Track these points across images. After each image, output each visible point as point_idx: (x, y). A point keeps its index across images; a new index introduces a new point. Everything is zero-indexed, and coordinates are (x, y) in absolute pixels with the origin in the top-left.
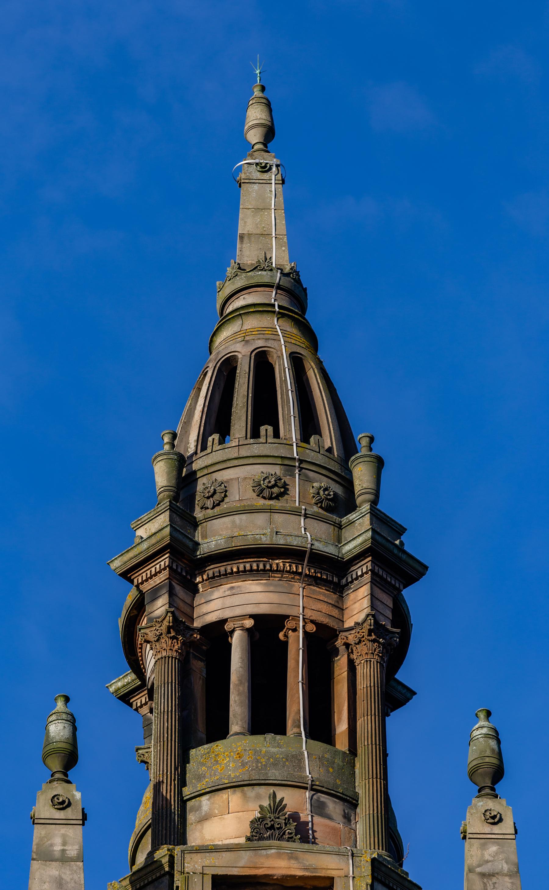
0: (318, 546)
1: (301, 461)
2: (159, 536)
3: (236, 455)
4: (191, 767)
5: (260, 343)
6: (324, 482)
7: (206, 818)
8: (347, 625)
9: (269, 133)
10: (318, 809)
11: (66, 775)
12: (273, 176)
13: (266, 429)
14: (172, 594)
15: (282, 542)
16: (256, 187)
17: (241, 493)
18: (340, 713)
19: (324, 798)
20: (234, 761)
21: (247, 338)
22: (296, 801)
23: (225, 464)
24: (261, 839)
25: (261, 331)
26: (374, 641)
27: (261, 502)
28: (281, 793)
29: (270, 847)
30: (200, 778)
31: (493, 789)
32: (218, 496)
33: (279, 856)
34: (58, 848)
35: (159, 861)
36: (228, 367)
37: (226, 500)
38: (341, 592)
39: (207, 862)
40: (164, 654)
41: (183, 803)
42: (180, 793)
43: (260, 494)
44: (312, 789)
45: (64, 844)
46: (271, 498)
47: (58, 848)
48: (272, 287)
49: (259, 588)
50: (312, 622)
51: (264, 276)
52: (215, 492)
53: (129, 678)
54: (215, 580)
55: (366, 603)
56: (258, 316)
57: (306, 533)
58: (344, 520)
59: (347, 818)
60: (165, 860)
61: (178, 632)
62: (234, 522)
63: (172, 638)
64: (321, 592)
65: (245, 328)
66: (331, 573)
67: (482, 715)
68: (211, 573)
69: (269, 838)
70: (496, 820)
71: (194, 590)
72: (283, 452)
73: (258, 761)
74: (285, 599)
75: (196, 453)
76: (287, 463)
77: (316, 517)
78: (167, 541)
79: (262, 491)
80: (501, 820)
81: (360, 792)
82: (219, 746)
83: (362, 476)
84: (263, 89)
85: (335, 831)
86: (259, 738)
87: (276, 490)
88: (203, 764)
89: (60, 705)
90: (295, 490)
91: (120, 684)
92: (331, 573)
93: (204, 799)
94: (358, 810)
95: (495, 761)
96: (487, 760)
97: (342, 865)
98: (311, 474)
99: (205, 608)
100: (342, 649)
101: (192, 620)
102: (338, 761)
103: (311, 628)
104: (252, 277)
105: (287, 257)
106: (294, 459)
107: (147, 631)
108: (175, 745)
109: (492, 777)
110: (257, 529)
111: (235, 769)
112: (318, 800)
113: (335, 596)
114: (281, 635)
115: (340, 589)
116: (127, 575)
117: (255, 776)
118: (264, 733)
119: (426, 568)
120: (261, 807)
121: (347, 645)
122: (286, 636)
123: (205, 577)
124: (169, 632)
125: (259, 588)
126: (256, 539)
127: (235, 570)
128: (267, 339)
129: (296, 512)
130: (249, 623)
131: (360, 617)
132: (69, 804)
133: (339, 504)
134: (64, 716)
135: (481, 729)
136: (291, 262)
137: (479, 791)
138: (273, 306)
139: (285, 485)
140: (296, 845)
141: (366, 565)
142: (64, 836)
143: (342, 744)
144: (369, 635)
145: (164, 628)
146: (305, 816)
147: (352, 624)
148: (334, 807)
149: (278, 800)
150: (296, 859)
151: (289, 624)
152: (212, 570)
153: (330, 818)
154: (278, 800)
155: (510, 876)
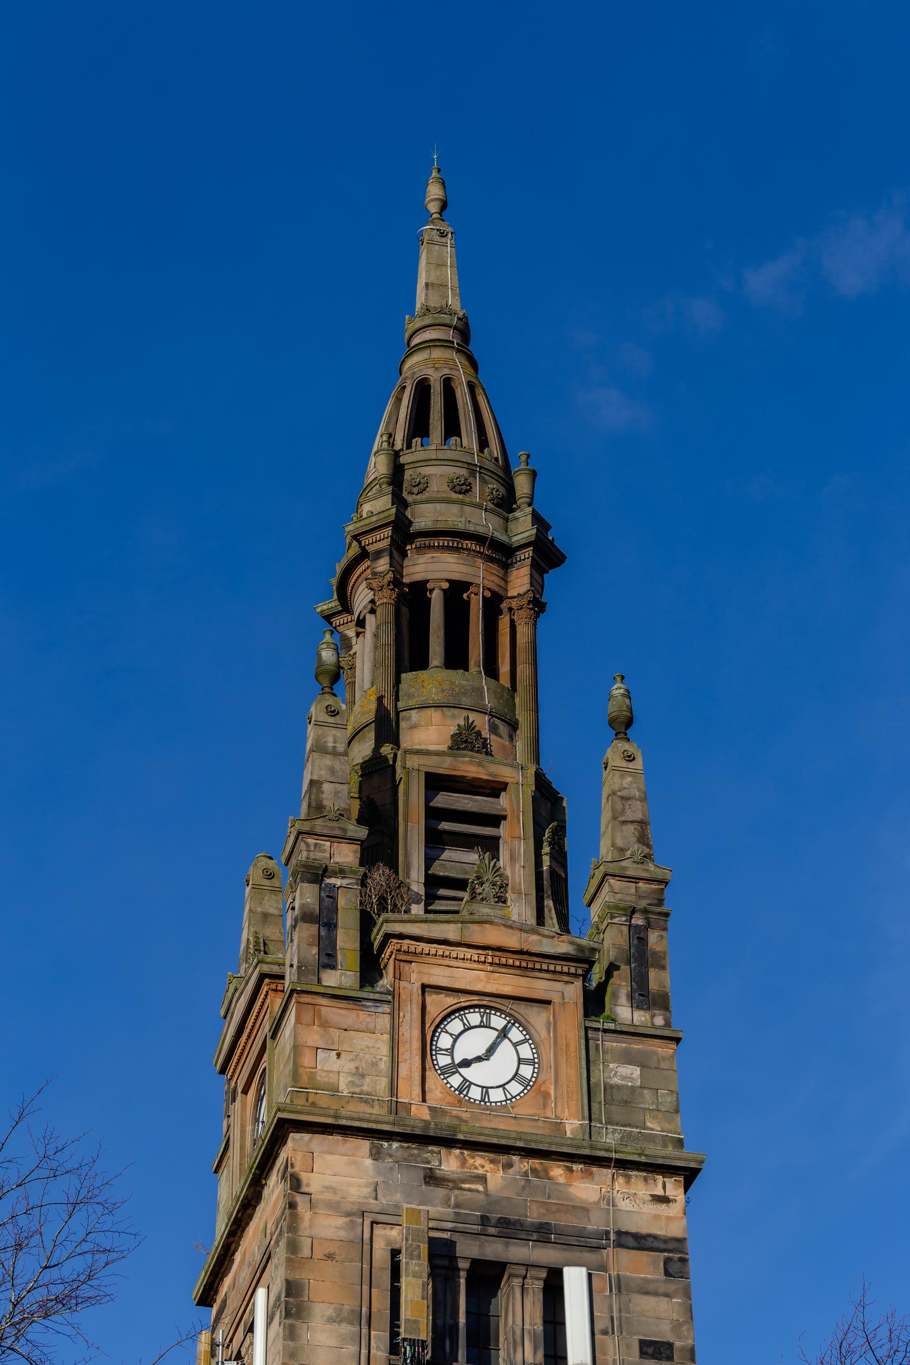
0: (497, 534)
1: (481, 467)
2: (386, 514)
3: (434, 457)
4: (403, 686)
5: (446, 371)
6: (495, 486)
7: (414, 727)
8: (509, 595)
9: (444, 206)
10: (494, 729)
11: (332, 689)
12: (448, 240)
13: (453, 440)
14: (391, 557)
15: (472, 529)
16: (437, 247)
17: (439, 487)
18: (503, 658)
19: (497, 721)
20: (436, 687)
21: (436, 366)
22: (481, 722)
23: (427, 462)
24: (459, 749)
25: (446, 361)
26: (531, 609)
27: (455, 496)
28: (473, 716)
29: (465, 756)
30: (410, 696)
31: (626, 734)
32: (422, 486)
33: (471, 763)
34: (330, 744)
35: (385, 757)
36: (423, 389)
37: (428, 489)
38: (507, 569)
39: (421, 762)
40: (385, 600)
41: (398, 713)
42: (396, 705)
43: (453, 489)
44: (490, 715)
45: (335, 742)
46: (460, 493)
47: (330, 744)
48: (451, 327)
49: (453, 560)
50: (489, 589)
51: (446, 319)
52: (420, 483)
53: (333, 604)
54: (420, 549)
55: (527, 580)
56: (442, 349)
57: (485, 523)
58: (511, 516)
59: (511, 738)
60: (390, 756)
61: (395, 586)
62: (435, 508)
63: (391, 590)
64: (494, 568)
65: (433, 357)
66: (501, 554)
67: (619, 679)
68: (418, 544)
69: (464, 749)
70: (630, 759)
71: (404, 555)
72: (467, 459)
73: (453, 690)
74: (471, 570)
75: (402, 449)
76: (471, 468)
77: (492, 512)
78: (393, 518)
79: (454, 487)
80: (634, 759)
81: (520, 719)
82: (423, 674)
83: (522, 484)
84: (439, 171)
85: (504, 746)
86: (452, 673)
87: (464, 487)
88: (412, 686)
89: (328, 637)
90: (477, 489)
91: (325, 607)
92: (501, 554)
93: (413, 712)
94: (518, 732)
95: (629, 714)
96: (624, 713)
97: (514, 774)
98: (487, 478)
99: (412, 570)
100: (505, 611)
101: (402, 576)
102: (505, 694)
103: (488, 594)
104: (437, 318)
105: (459, 305)
106: (476, 465)
107: (372, 581)
108: (392, 670)
109: (623, 726)
110: (452, 516)
111: (437, 693)
112: (493, 723)
113: (503, 572)
114: (465, 596)
115: (506, 566)
116: (355, 537)
117: (452, 701)
118: (456, 669)
119: (565, 558)
120: (459, 726)
121: (510, 609)
122: (468, 597)
123: (414, 546)
124: (389, 585)
125: (453, 560)
126: (454, 525)
127: (436, 544)
128: (451, 369)
129: (479, 506)
130: (446, 585)
131: (523, 590)
132: (338, 713)
133: (506, 503)
134: (332, 646)
135: (618, 690)
136: (462, 309)
137: (616, 735)
138: (453, 342)
139: (470, 484)
140: (482, 756)
141: (529, 552)
142: (334, 736)
143: (505, 680)
144: (528, 604)
145: (385, 581)
146: (485, 734)
147: (516, 594)
148: (503, 729)
149: (470, 721)
150: (483, 766)
151: (472, 589)
152: (419, 542)
153: (501, 737)
154: (470, 721)
155: (640, 801)
